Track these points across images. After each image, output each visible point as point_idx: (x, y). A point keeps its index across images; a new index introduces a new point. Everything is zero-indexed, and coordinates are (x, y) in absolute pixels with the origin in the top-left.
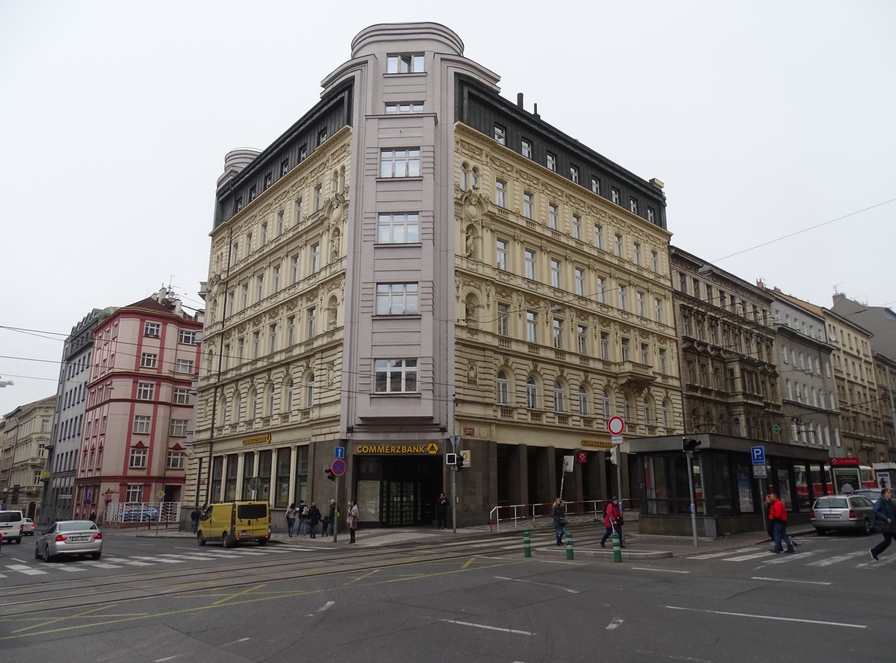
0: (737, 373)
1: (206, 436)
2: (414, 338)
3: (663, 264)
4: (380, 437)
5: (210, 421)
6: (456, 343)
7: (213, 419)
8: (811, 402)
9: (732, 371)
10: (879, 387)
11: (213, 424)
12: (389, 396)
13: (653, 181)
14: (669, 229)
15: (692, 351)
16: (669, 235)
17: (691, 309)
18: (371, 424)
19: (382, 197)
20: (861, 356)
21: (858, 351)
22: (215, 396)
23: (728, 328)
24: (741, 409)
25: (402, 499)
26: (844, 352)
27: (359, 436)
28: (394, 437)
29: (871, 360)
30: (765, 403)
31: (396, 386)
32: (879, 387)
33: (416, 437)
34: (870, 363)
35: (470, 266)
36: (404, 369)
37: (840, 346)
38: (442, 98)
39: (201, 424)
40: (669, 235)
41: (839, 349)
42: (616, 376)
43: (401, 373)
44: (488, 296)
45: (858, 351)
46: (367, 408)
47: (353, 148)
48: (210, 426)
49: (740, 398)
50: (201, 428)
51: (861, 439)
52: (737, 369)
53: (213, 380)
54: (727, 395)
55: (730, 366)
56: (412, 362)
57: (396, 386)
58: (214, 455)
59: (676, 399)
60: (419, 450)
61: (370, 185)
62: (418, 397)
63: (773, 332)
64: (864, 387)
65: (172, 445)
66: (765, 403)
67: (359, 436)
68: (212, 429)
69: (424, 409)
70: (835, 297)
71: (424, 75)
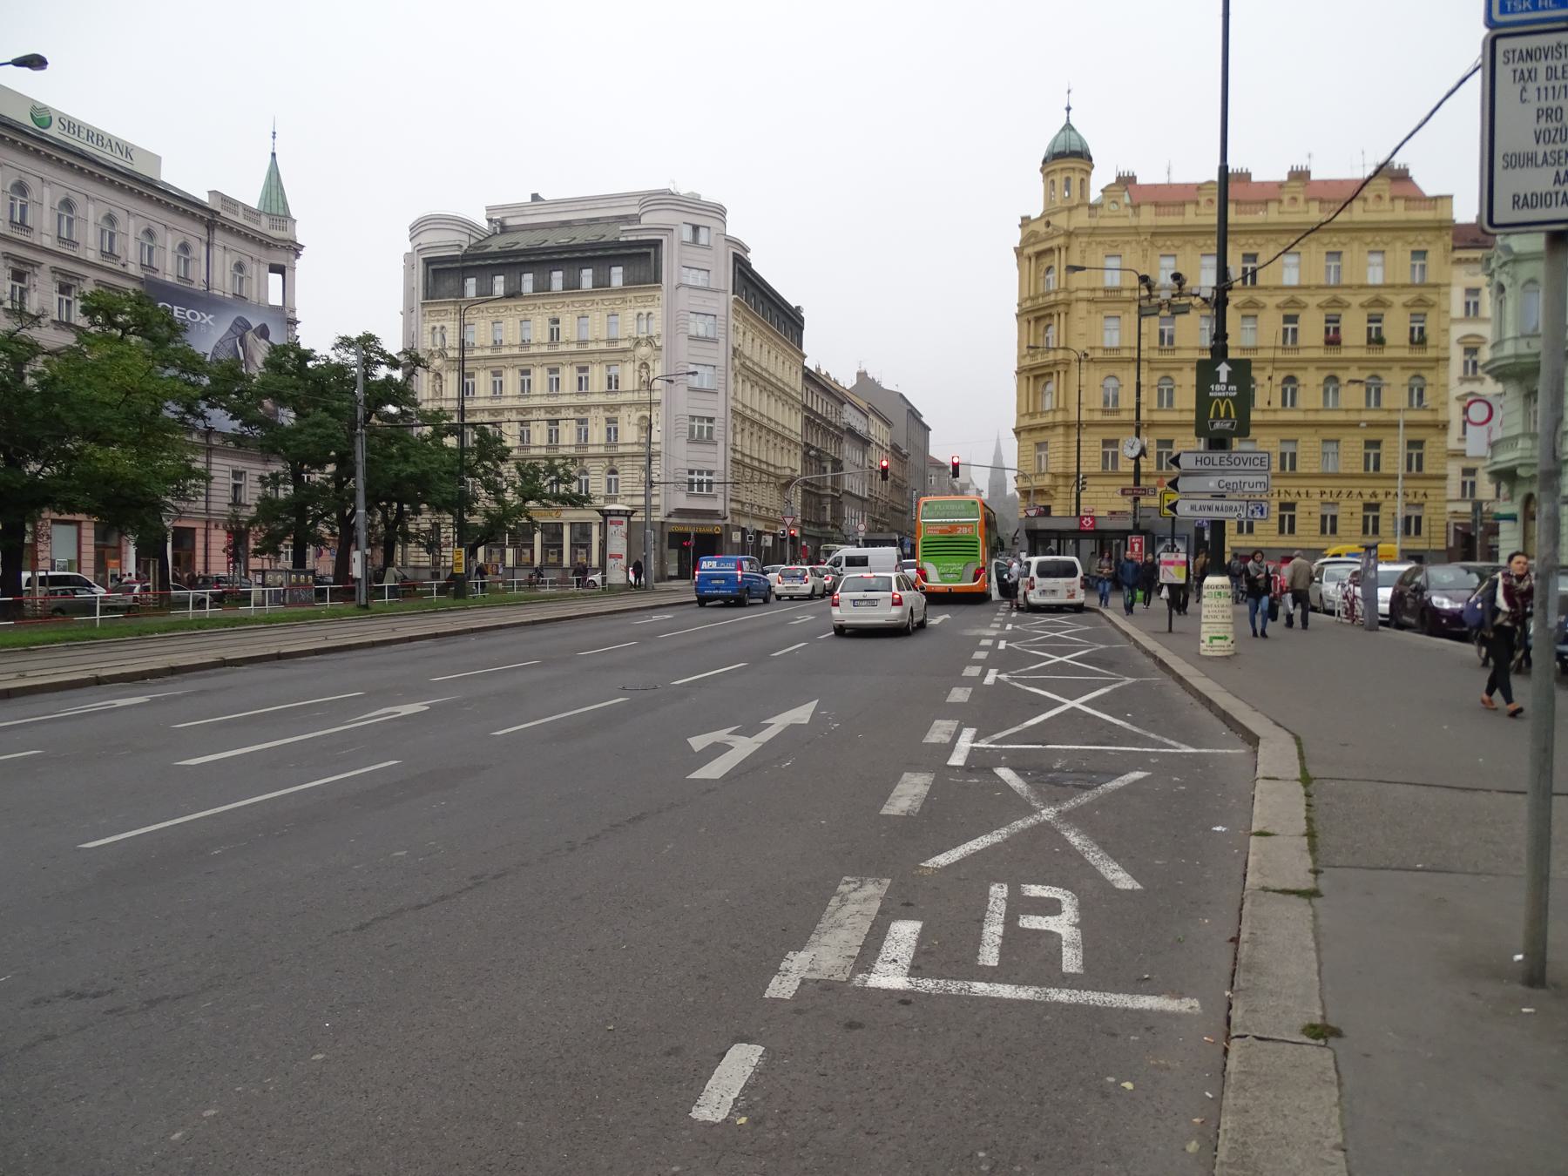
2: (712, 457)
3: (796, 382)
4: (685, 521)
13: (798, 308)
14: (805, 350)
16: (804, 357)
17: (812, 421)
18: (681, 512)
19: (693, 351)
25: (343, 564)
27: (672, 520)
28: (694, 521)
33: (707, 522)
38: (724, 276)
40: (804, 357)
42: (778, 477)
46: (682, 501)
49: (829, 491)
54: (818, 488)
60: (709, 530)
61: (683, 341)
62: (715, 497)
63: (843, 432)
67: (672, 520)
69: (718, 505)
70: (859, 374)
71: (708, 247)
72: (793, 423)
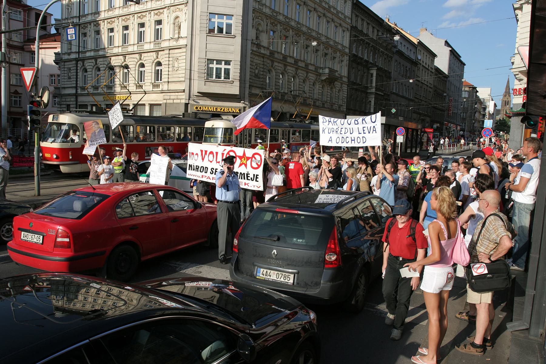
0: (375, 75)
1: (73, 91)
5: (75, 82)
6: (251, 53)
7: (77, 81)
8: (403, 93)
9: (372, 75)
10: (434, 86)
11: (77, 84)
12: (223, 82)
15: (355, 61)
20: (430, 69)
21: (429, 66)
22: (77, 67)
23: (375, 50)
24: (373, 96)
26: (423, 66)
29: (433, 71)
30: (384, 94)
31: (218, 76)
32: (434, 86)
34: (432, 73)
35: (260, 7)
36: (223, 66)
37: (421, 62)
39: (65, 83)
41: (421, 64)
43: (225, 69)
44: (267, 25)
45: (429, 66)
47: (517, 214)
48: (75, 85)
50: (66, 86)
51: (420, 114)
52: (374, 72)
53: (73, 56)
55: (372, 72)
56: (227, 63)
57: (218, 76)
58: (78, 103)
59: (345, 87)
64: (427, 86)
65: (12, 91)
66: (384, 94)
68: (76, 88)
72: (344, 39)
